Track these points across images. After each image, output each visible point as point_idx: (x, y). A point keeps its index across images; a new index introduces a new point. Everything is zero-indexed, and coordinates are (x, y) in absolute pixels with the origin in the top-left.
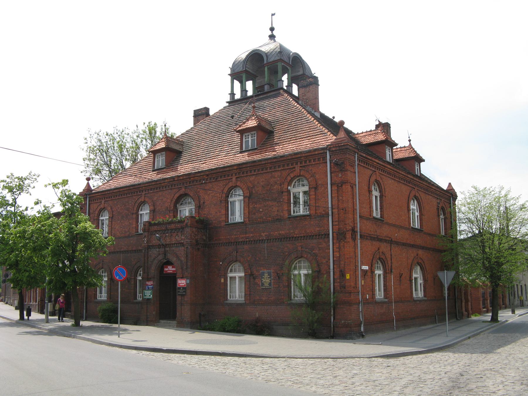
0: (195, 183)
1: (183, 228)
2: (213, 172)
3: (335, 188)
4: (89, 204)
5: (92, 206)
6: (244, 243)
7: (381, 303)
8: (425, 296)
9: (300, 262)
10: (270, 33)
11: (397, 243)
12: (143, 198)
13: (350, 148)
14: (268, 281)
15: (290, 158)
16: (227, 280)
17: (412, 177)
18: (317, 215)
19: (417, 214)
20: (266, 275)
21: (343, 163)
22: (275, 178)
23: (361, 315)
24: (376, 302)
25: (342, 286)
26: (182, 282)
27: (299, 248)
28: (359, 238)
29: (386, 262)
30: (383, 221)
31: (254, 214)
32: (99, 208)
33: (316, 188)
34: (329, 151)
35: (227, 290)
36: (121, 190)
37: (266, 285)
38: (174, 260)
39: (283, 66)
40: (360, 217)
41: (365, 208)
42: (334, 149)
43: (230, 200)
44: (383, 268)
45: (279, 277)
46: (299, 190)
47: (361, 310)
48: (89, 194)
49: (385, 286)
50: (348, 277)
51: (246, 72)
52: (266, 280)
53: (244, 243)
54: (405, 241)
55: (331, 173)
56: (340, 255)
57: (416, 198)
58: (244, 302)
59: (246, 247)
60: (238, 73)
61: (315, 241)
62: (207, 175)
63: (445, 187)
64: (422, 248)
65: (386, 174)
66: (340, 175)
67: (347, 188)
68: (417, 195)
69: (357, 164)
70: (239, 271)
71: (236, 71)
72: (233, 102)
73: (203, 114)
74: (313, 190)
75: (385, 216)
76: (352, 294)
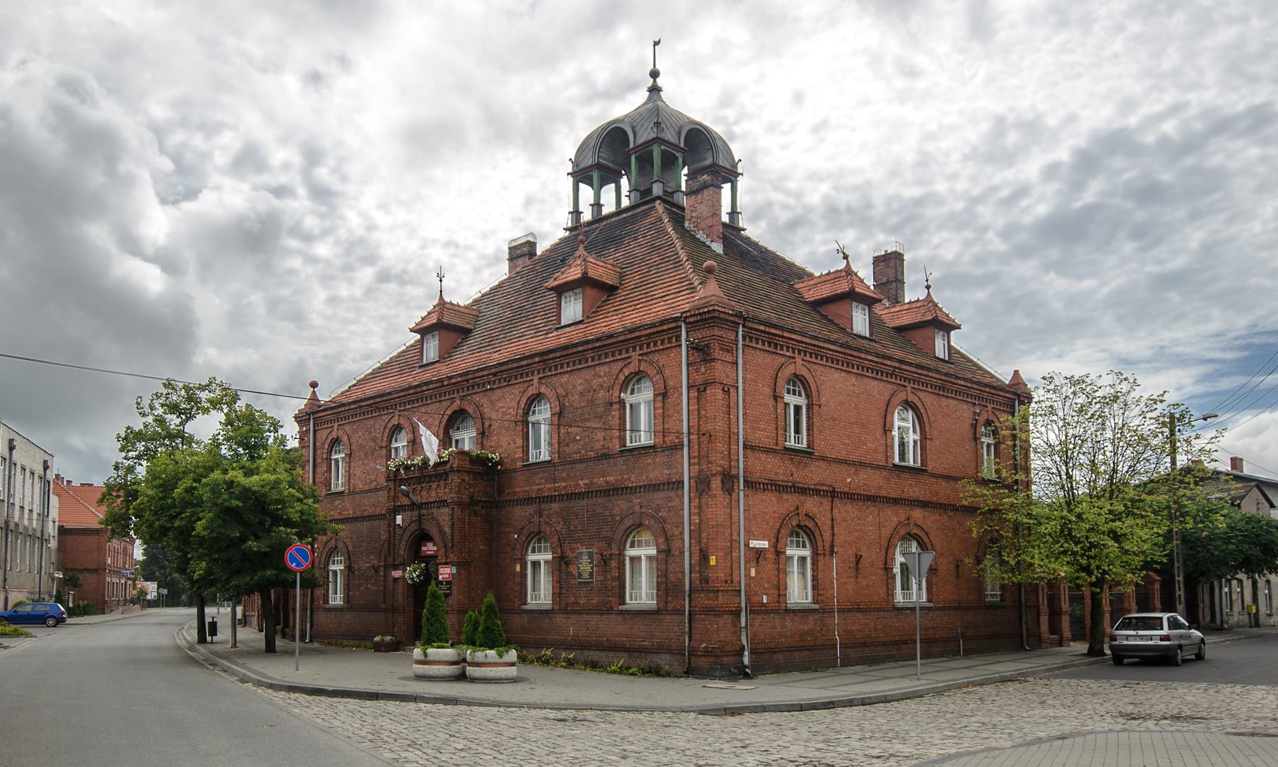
0: (476, 390)
1: (446, 473)
3: (694, 394)
4: (315, 431)
5: (319, 434)
6: (551, 499)
7: (804, 612)
9: (539, 542)
11: (850, 496)
13: (722, 316)
14: (588, 569)
16: (624, 565)
17: (898, 365)
18: (667, 447)
19: (912, 437)
21: (707, 346)
22: (600, 377)
24: (787, 611)
25: (703, 582)
26: (445, 572)
27: (637, 508)
28: (742, 487)
29: (816, 533)
30: (812, 453)
32: (330, 438)
33: (664, 395)
34: (687, 324)
35: (526, 586)
37: (586, 575)
38: (434, 532)
39: (663, 152)
40: (745, 447)
41: (764, 430)
42: (692, 320)
43: (532, 419)
45: (605, 561)
46: (642, 398)
47: (743, 624)
48: (314, 413)
49: (814, 578)
50: (713, 562)
51: (598, 166)
52: (585, 566)
53: (551, 499)
54: (873, 492)
55: (688, 365)
56: (701, 520)
57: (908, 405)
58: (550, 607)
59: (555, 506)
60: (587, 172)
61: (662, 494)
62: (495, 374)
63: (1007, 379)
64: (924, 504)
65: (824, 362)
66: (703, 369)
67: (715, 393)
68: (912, 398)
69: (740, 346)
70: (647, 544)
71: (582, 166)
72: (576, 227)
74: (660, 398)
75: (817, 442)
76: (720, 594)
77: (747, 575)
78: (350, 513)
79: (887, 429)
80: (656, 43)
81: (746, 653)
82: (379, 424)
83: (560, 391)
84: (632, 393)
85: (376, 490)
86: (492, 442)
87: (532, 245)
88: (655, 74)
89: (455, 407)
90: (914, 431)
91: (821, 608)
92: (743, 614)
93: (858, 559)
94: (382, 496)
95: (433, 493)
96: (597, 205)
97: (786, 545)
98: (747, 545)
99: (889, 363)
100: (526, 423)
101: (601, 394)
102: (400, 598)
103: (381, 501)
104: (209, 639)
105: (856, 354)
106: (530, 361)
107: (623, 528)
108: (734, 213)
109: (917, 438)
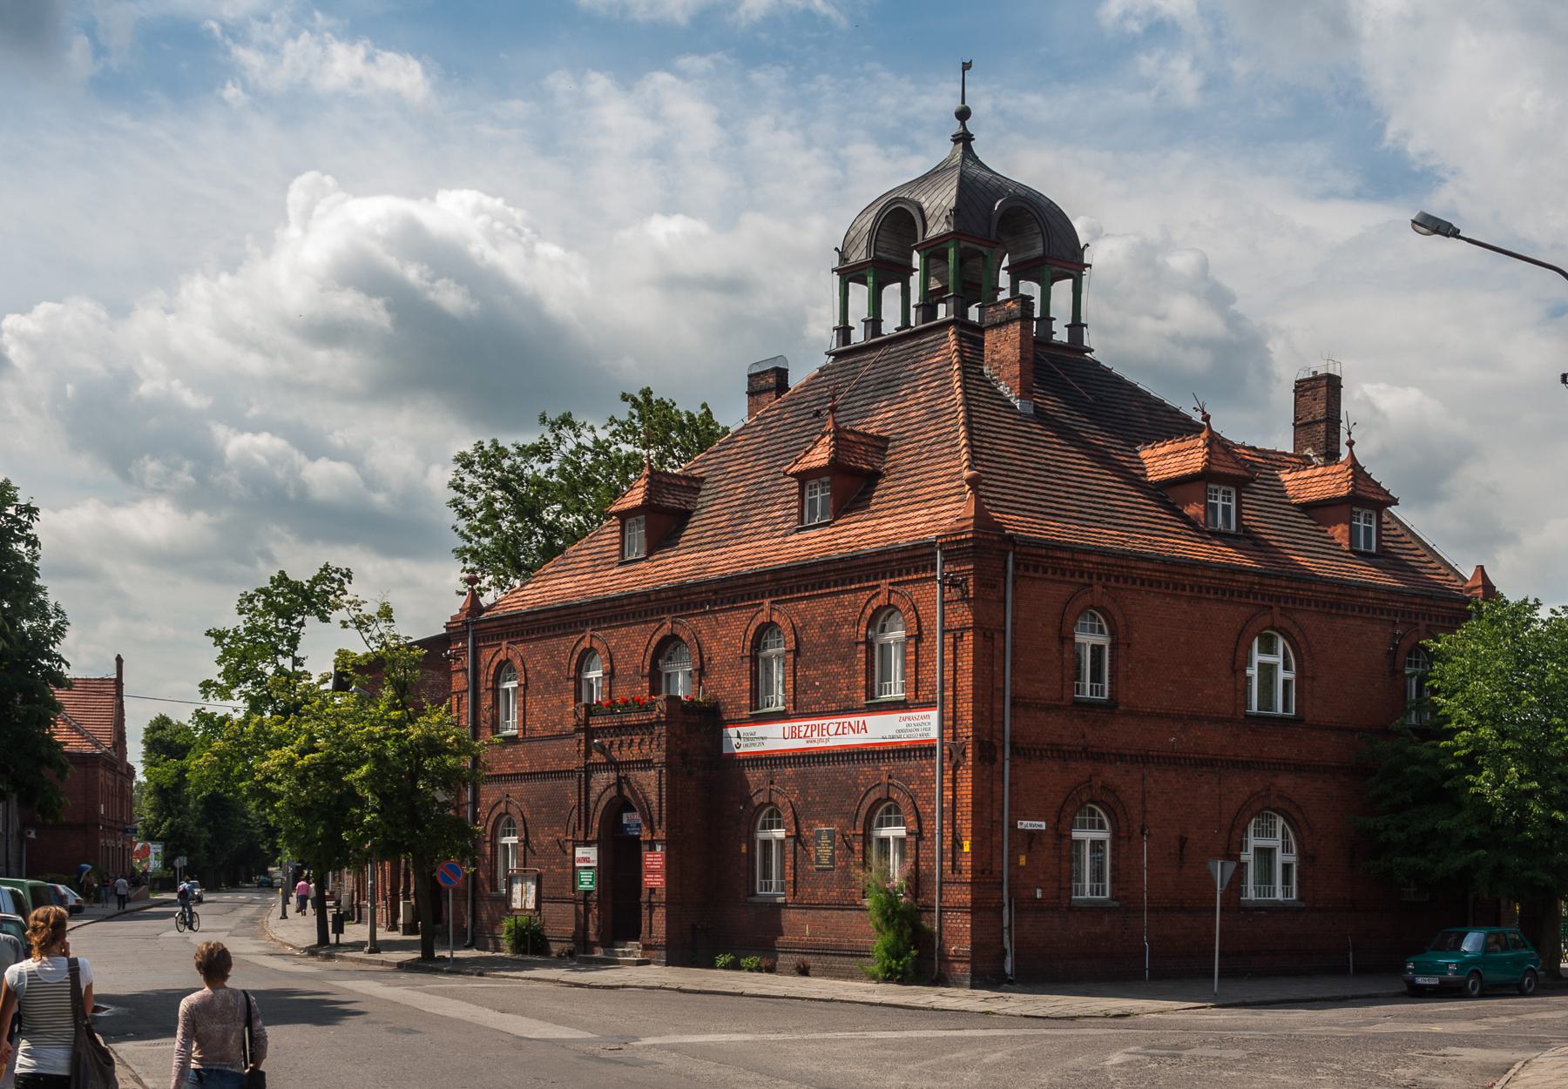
2: (728, 584)
3: (949, 639)
8: (1300, 898)
10: (956, 127)
12: (588, 638)
14: (828, 852)
15: (869, 560)
20: (824, 839)
22: (845, 607)
23: (1006, 937)
27: (884, 779)
31: (805, 692)
32: (497, 660)
36: (542, 616)
37: (825, 860)
43: (763, 654)
44: (1112, 824)
47: (1006, 924)
48: (474, 624)
55: (943, 603)
62: (715, 592)
72: (845, 353)
73: (770, 390)
77: (1013, 863)
78: (525, 767)
79: (1238, 665)
80: (966, 67)
81: (1009, 959)
82: (565, 646)
83: (796, 620)
84: (883, 630)
85: (559, 737)
86: (712, 681)
87: (781, 374)
88: (963, 115)
89: (665, 630)
90: (1286, 667)
91: (1125, 903)
92: (1006, 911)
93: (1183, 841)
94: (570, 746)
95: (635, 749)
96: (874, 323)
97: (1072, 826)
98: (1013, 826)
99: (1241, 578)
100: (754, 659)
101: (846, 629)
102: (139, 769)
103: (569, 754)
104: (332, 938)
105: (1187, 571)
106: (760, 579)
107: (868, 802)
108: (1076, 327)
109: (1291, 676)
